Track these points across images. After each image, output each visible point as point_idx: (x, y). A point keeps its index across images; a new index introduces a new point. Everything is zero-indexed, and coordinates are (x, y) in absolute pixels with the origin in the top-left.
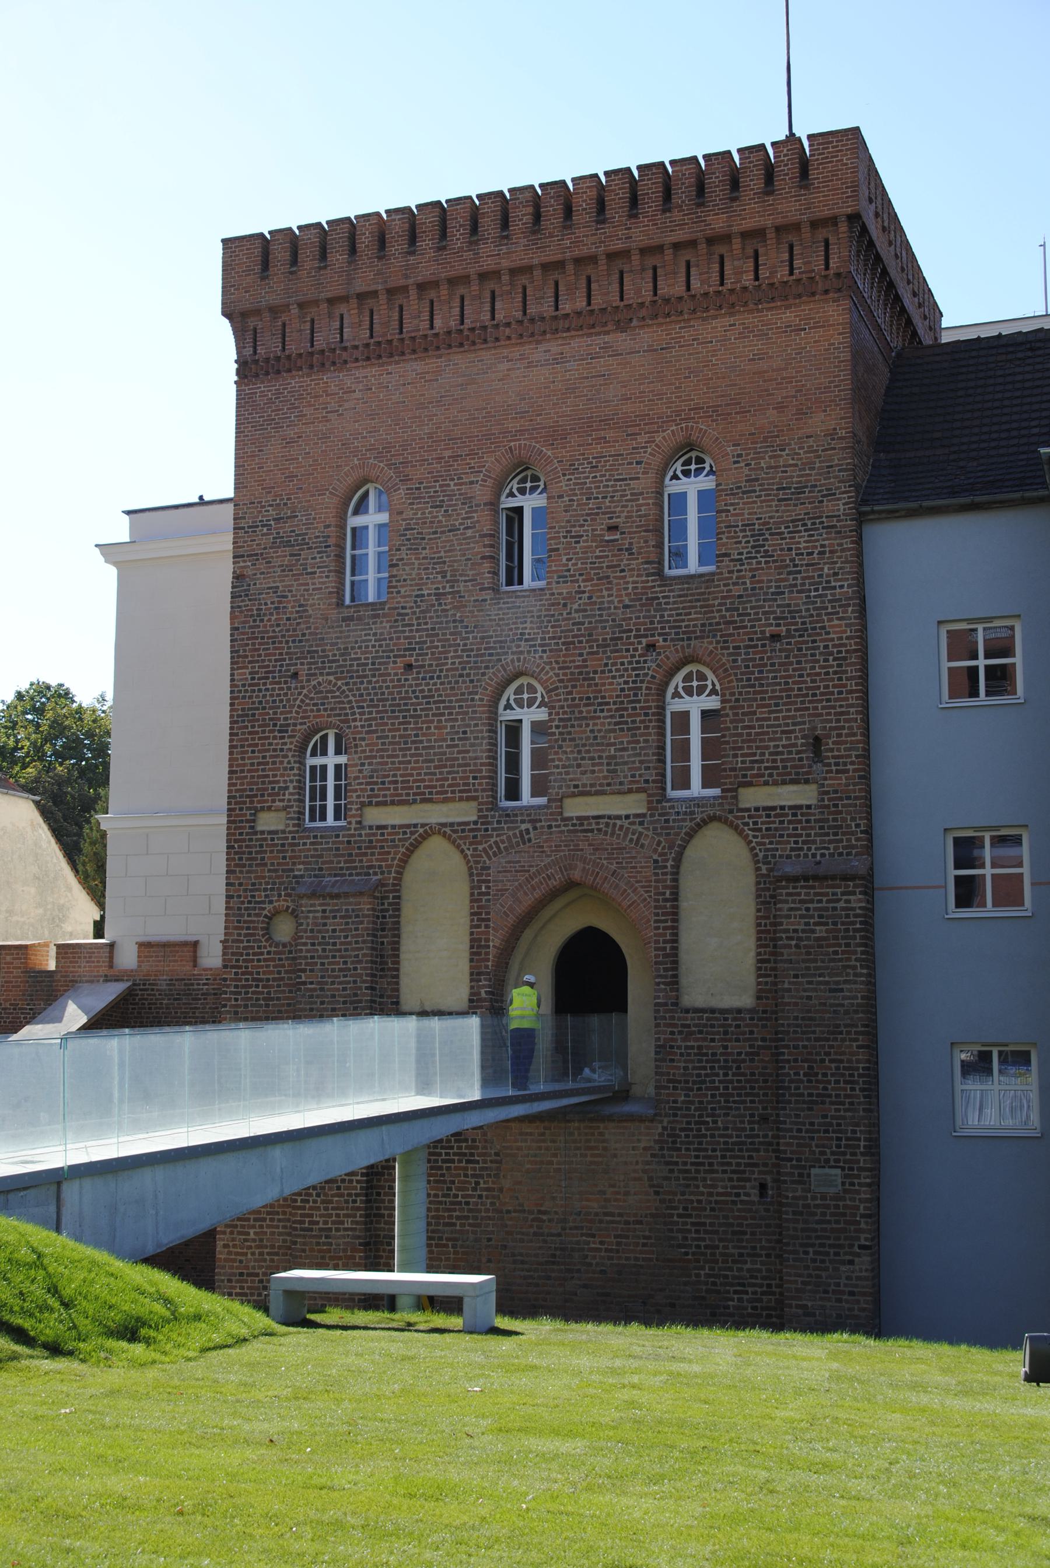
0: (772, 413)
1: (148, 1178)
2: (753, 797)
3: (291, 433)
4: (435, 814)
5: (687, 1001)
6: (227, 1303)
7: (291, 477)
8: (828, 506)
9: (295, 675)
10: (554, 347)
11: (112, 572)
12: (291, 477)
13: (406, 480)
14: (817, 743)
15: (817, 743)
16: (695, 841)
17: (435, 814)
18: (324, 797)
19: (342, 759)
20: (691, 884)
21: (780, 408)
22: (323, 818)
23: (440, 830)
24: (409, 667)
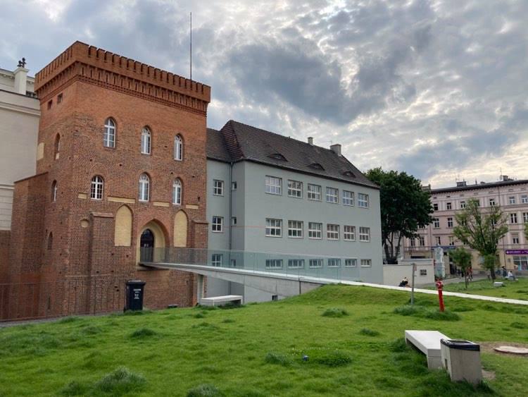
0: (194, 134)
1: (358, 280)
2: (188, 207)
3: (93, 99)
4: (126, 201)
5: (116, 245)
6: (49, 321)
7: (92, 110)
8: (203, 155)
9: (91, 160)
10: (155, 104)
11: (219, 130)
12: (92, 110)
13: (122, 121)
14: (199, 198)
15: (199, 198)
16: (185, 216)
17: (126, 201)
18: (98, 190)
19: (100, 183)
20: (176, 222)
21: (196, 133)
22: (94, 197)
23: (126, 205)
24: (121, 165)
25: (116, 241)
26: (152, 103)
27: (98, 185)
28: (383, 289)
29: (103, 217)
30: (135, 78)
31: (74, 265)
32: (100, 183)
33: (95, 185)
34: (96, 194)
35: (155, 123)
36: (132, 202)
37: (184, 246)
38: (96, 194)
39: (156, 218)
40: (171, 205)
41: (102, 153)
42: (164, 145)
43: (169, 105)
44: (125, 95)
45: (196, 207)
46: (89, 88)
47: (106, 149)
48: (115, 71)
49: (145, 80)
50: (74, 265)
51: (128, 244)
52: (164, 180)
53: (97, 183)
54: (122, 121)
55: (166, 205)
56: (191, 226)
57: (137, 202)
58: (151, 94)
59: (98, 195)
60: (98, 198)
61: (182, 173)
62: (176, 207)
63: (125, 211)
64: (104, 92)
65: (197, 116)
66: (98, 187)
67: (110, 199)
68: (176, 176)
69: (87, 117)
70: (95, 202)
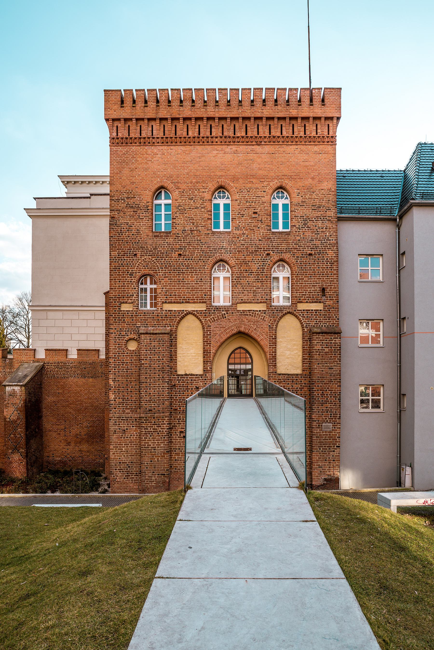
2: (301, 307)
3: (133, 167)
4: (190, 307)
5: (179, 373)
8: (329, 213)
10: (234, 148)
12: (133, 183)
15: (323, 290)
17: (190, 307)
19: (154, 286)
21: (313, 179)
22: (146, 306)
24: (180, 255)
25: (179, 368)
26: (228, 149)
27: (151, 289)
28: (65, 507)
29: (156, 334)
30: (217, 115)
31: (121, 400)
32: (154, 286)
33: (146, 289)
34: (148, 301)
35: (235, 179)
36: (202, 307)
37: (299, 371)
38: (148, 301)
39: (242, 329)
40: (269, 306)
41: (150, 242)
42: (251, 211)
43: (259, 144)
44: (183, 148)
45: (319, 307)
46: (127, 152)
47: (158, 235)
48: (161, 115)
49: (211, 115)
50: (121, 400)
51: (198, 370)
52: (255, 267)
53: (149, 286)
54: (178, 188)
55: (262, 307)
56: (309, 336)
57: (210, 307)
58: (226, 134)
59: (151, 304)
60: (151, 307)
61: (288, 251)
62: (281, 309)
63: (190, 321)
64: (149, 152)
65: (316, 148)
66: (151, 292)
67: (167, 307)
68: (276, 258)
69: (126, 195)
70: (148, 312)
